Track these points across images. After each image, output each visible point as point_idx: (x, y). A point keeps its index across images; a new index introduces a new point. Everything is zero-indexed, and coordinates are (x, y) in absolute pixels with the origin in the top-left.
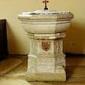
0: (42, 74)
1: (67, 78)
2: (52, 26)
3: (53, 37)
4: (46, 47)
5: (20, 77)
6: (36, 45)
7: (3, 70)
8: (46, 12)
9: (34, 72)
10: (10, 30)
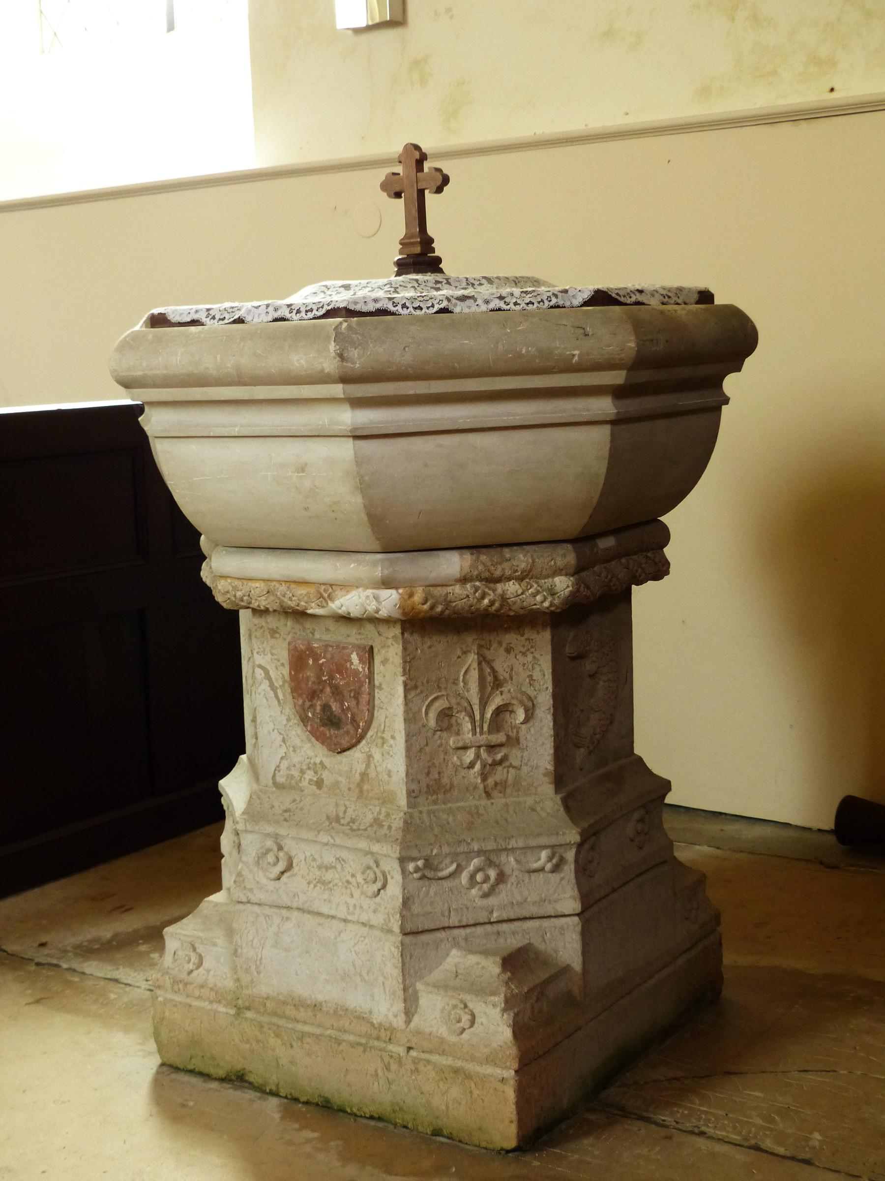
0: (284, 1009)
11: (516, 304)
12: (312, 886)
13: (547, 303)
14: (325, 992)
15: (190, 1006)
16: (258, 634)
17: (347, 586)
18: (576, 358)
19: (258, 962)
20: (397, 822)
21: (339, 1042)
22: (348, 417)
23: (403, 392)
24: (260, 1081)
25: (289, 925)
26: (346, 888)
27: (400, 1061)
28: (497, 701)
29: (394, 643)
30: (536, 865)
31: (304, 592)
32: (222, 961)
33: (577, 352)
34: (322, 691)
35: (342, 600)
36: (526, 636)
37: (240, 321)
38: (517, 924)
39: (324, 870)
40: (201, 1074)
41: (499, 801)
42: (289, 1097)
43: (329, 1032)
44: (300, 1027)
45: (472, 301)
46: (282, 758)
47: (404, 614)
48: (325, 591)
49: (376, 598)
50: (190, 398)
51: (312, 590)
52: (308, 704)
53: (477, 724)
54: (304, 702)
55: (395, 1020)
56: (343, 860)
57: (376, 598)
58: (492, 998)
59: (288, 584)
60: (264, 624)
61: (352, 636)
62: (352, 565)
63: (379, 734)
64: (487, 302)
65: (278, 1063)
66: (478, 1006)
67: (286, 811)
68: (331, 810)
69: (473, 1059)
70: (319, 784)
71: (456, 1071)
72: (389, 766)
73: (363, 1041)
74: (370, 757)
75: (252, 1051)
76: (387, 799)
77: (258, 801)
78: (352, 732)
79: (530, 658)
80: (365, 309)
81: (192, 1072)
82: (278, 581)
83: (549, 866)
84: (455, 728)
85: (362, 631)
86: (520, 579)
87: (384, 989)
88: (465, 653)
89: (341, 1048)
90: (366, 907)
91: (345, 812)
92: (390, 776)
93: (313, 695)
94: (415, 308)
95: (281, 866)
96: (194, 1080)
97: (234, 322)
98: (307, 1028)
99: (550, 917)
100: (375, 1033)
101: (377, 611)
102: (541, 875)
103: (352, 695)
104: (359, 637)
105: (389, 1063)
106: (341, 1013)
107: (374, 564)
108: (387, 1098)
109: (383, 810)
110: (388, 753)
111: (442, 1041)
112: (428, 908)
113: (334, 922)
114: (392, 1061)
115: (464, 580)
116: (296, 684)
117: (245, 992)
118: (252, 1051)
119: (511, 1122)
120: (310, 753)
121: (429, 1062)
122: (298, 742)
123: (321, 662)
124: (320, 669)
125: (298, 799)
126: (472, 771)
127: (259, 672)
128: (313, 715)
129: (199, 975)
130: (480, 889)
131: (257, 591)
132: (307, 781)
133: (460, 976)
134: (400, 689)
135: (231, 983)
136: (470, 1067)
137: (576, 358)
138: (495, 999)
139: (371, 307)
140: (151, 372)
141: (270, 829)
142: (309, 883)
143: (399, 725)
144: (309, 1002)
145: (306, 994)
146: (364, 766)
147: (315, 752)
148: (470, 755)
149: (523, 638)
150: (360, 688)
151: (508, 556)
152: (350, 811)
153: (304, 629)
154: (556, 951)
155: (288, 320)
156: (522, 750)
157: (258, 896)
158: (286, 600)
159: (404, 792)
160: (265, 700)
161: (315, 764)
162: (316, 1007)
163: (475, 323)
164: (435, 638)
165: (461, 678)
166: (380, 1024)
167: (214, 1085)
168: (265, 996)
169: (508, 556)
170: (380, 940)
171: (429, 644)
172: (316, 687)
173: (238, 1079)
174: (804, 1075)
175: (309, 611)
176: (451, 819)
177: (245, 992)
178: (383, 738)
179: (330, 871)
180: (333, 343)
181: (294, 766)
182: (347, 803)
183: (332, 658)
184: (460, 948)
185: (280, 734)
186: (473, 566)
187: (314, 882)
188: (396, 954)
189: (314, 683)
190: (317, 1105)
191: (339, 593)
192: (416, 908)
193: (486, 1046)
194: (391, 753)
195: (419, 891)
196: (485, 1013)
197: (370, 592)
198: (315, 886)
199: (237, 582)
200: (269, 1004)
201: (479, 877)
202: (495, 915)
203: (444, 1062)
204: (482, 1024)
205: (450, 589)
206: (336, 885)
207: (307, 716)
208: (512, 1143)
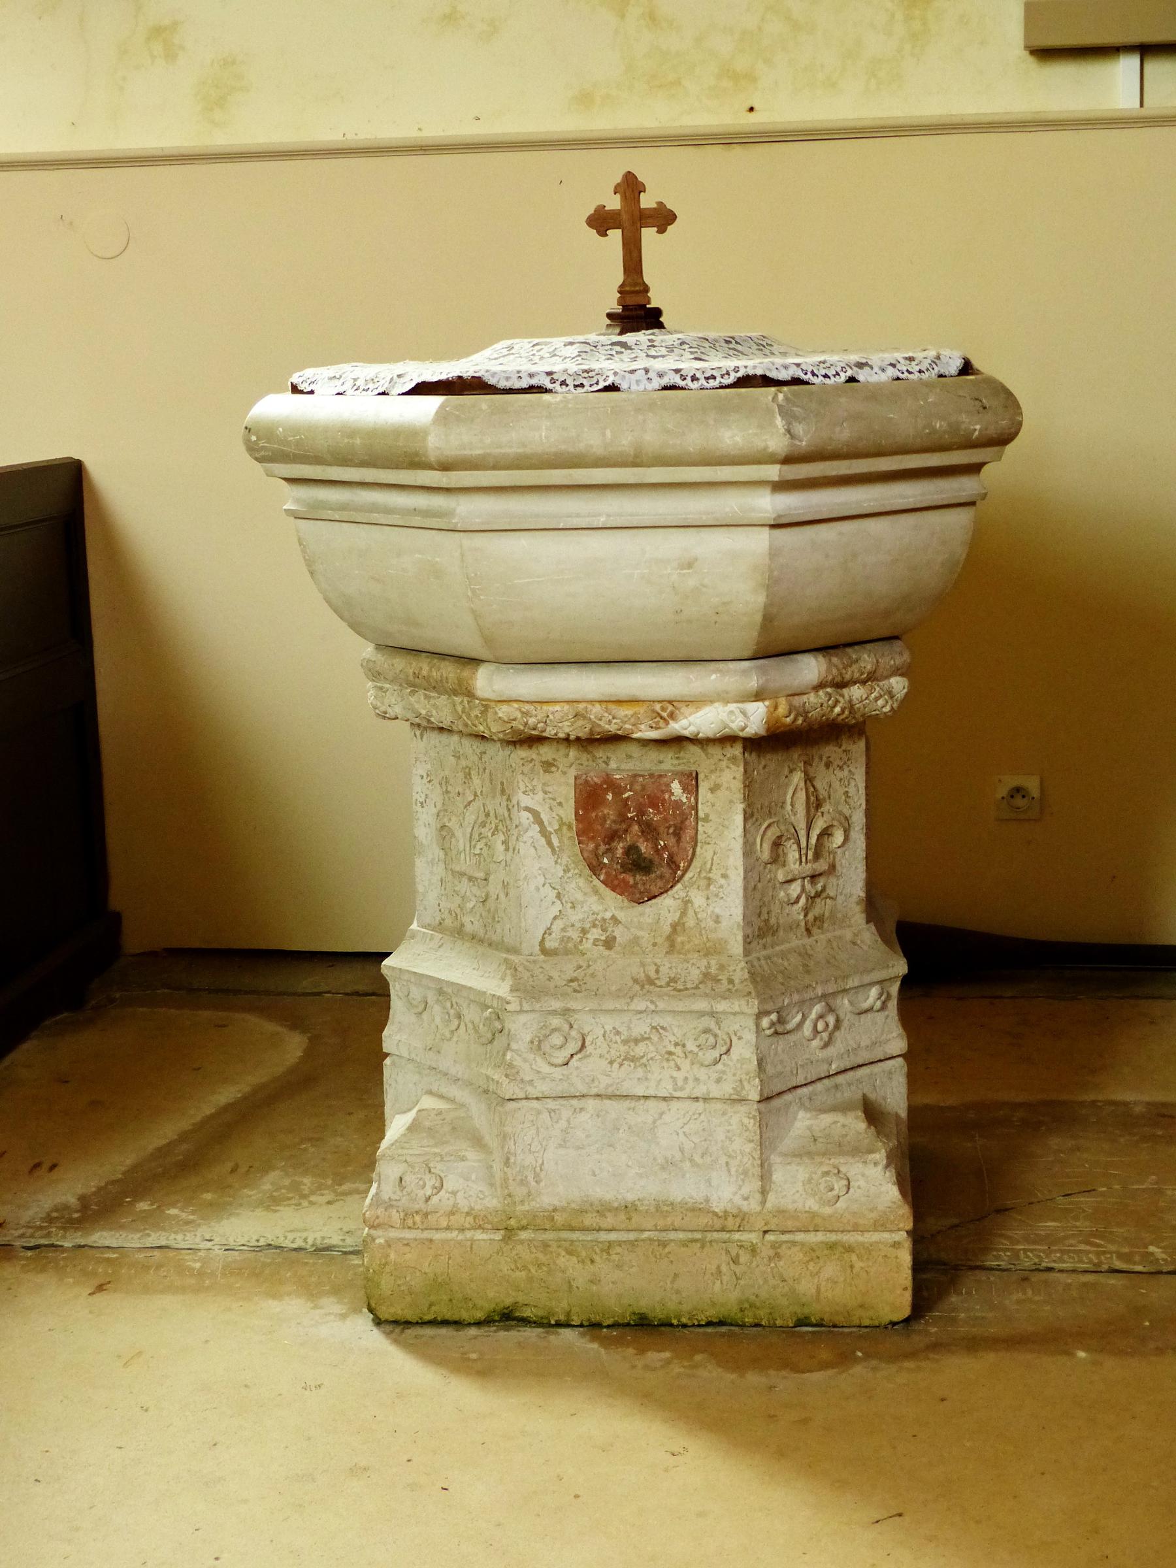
0: (573, 1224)
1: (940, 1265)
2: (722, 554)
3: (725, 704)
4: (633, 844)
5: (273, 1268)
6: (502, 824)
7: (41, 1167)
8: (643, 360)
9: (465, 1185)
10: (93, 491)
12: (616, 1065)
13: (842, 374)
14: (639, 1186)
15: (431, 1240)
16: (526, 769)
18: (977, 433)
19: (538, 1169)
20: (739, 972)
21: (664, 1244)
22: (768, 504)
23: (873, 469)
24: (541, 1313)
25: (584, 1117)
26: (668, 1060)
27: (753, 1250)
28: (819, 825)
30: (866, 1005)
31: (630, 712)
32: (473, 1177)
33: (978, 427)
34: (626, 831)
35: (691, 718)
36: (843, 748)
37: (612, 388)
38: (851, 1074)
39: (632, 1044)
40: (445, 1323)
41: (821, 937)
42: (585, 1323)
43: (646, 1235)
44: (604, 1236)
46: (555, 918)
47: (768, 730)
48: (663, 709)
49: (744, 713)
51: (641, 710)
52: (603, 848)
53: (803, 852)
54: (597, 847)
55: (745, 1203)
56: (662, 1028)
57: (744, 713)
58: (873, 1156)
59: (604, 705)
60: (534, 756)
61: (668, 761)
62: (714, 677)
63: (703, 874)
64: (661, 375)
65: (570, 1286)
66: (853, 1168)
67: (571, 981)
68: (636, 971)
69: (856, 1228)
70: (609, 943)
71: (832, 1246)
72: (717, 910)
73: (698, 1236)
74: (687, 902)
75: (530, 1279)
76: (712, 949)
77: (528, 974)
78: (667, 875)
79: (846, 772)
80: (518, 385)
81: (433, 1323)
82: (592, 702)
83: (878, 1004)
84: (782, 859)
85: (682, 754)
86: (864, 682)
87: (729, 1171)
88: (791, 771)
89: (667, 1250)
91: (657, 971)
93: (612, 837)
94: (707, 379)
95: (573, 1046)
96: (443, 1331)
97: (665, 388)
98: (613, 1236)
99: (880, 1061)
101: (743, 729)
102: (869, 1015)
103: (671, 831)
104: (676, 762)
105: (738, 1255)
106: (666, 1208)
107: (745, 672)
108: (733, 1296)
109: (713, 962)
110: (717, 895)
111: (813, 1215)
112: (779, 1068)
113: (651, 1103)
114: (741, 1252)
115: (818, 687)
116: (586, 827)
117: (519, 1208)
118: (530, 1279)
119: (905, 1289)
120: (596, 907)
121: (794, 1243)
122: (579, 896)
125: (585, 965)
126: (796, 907)
127: (525, 818)
128: (611, 860)
129: (442, 1200)
130: (821, 1039)
131: (558, 716)
133: (820, 1140)
134: (739, 819)
135: (495, 1201)
137: (977, 433)
138: (877, 1156)
139: (524, 384)
140: (498, 451)
141: (556, 1005)
142: (611, 1063)
143: (735, 864)
144: (616, 1205)
145: (609, 1196)
146: (678, 914)
147: (611, 904)
148: (795, 889)
149: (840, 750)
150: (682, 822)
151: (854, 657)
153: (594, 759)
154: (885, 1099)
156: (838, 877)
157: (542, 1088)
158: (601, 723)
159: (740, 938)
160: (533, 850)
161: (604, 920)
162: (629, 1209)
163: (875, 394)
164: (769, 756)
165: (789, 800)
166: (726, 1212)
167: (473, 1331)
168: (551, 1208)
169: (854, 657)
171: (763, 763)
172: (615, 827)
173: (507, 1318)
174: (1068, 1199)
175: (634, 736)
176: (786, 964)
177: (519, 1208)
179: (641, 1044)
180: (779, 418)
181: (573, 925)
182: (658, 961)
183: (644, 788)
184: (807, 1110)
186: (828, 670)
187: (619, 1060)
188: (750, 1126)
189: (614, 822)
190: (628, 1325)
191: (684, 709)
192: (770, 1070)
193: (871, 1210)
194: (721, 895)
195: (769, 1048)
196: (863, 1175)
197: (732, 706)
198: (621, 1065)
199: (527, 707)
201: (820, 1026)
202: (834, 1066)
204: (859, 1187)
205: (805, 698)
207: (601, 864)
208: (906, 1312)
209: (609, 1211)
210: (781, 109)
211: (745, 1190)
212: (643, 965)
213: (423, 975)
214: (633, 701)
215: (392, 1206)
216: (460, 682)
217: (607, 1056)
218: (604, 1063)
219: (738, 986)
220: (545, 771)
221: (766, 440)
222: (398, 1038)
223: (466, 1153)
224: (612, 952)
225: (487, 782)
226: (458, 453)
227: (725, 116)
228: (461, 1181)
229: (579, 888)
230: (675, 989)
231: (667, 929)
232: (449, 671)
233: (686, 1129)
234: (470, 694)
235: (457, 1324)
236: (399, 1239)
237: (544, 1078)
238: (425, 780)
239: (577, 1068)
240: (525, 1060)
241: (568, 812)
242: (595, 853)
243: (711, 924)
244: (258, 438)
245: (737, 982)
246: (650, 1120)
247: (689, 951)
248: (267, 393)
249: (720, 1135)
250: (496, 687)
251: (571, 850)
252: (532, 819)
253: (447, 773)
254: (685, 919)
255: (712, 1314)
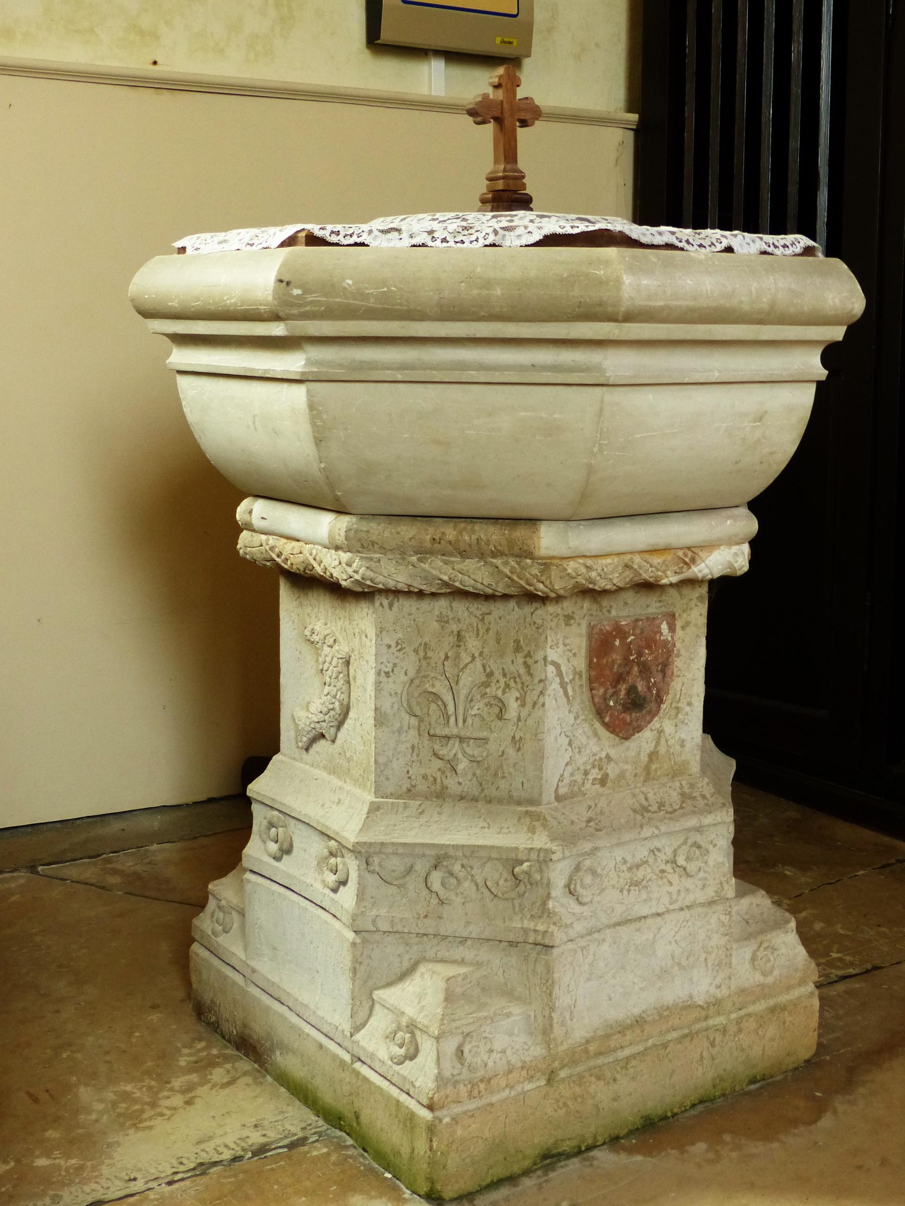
11: (444, 240)
12: (625, 892)
14: (641, 1000)
15: (492, 1105)
17: (710, 546)
21: (665, 1046)
24: (574, 1143)
25: (605, 947)
26: (661, 878)
29: (699, 604)
32: (516, 1031)
34: (628, 673)
39: (634, 870)
45: (396, 233)
46: (567, 764)
48: (686, 555)
50: (689, 337)
51: (669, 557)
54: (605, 692)
60: (559, 611)
62: (729, 522)
72: (683, 736)
73: (686, 1031)
74: (661, 732)
76: (678, 772)
85: (664, 597)
87: (706, 966)
89: (667, 1051)
90: (692, 887)
91: (646, 799)
92: (682, 746)
93: (619, 678)
98: (627, 1052)
100: (703, 1013)
104: (659, 605)
106: (665, 1014)
109: (684, 783)
111: (763, 986)
113: (650, 921)
120: (595, 749)
121: (750, 1015)
123: (629, 640)
124: (628, 648)
125: (593, 805)
131: (610, 568)
132: (590, 782)
133: (750, 921)
135: (538, 1049)
136: (783, 999)
140: (675, 303)
142: (621, 891)
144: (629, 1022)
146: (654, 744)
150: (668, 659)
152: (650, 796)
155: (499, 246)
158: (641, 572)
161: (601, 759)
162: (639, 1022)
166: (707, 1003)
168: (583, 1041)
170: (706, 915)
172: (621, 671)
178: (677, 708)
179: (641, 868)
181: (579, 769)
183: (642, 632)
185: (567, 736)
187: (627, 887)
189: (620, 665)
194: (686, 721)
196: (784, 943)
198: (629, 891)
199: (589, 562)
200: (592, 1048)
203: (761, 1008)
206: (650, 879)
209: (627, 1029)
210: (179, 63)
211: (718, 980)
212: (634, 795)
213: (415, 844)
214: (666, 549)
215: (457, 1082)
216: (511, 543)
217: (617, 885)
218: (616, 893)
219: (712, 800)
220: (566, 625)
221: (853, 303)
222: (374, 912)
223: (511, 1009)
224: (605, 789)
225: (492, 642)
226: (647, 303)
227: (134, 62)
228: (507, 1037)
229: (584, 732)
230: (667, 812)
231: (644, 758)
232: (493, 535)
233: (677, 937)
234: (530, 555)
235: (511, 1179)
236: (465, 1113)
237: (578, 919)
238: (393, 649)
239: (599, 902)
240: (562, 906)
241: (581, 663)
242: (605, 699)
243: (678, 747)
244: (306, 291)
245: (708, 796)
246: (651, 936)
247: (660, 777)
248: (147, 258)
249: (702, 935)
250: (571, 544)
251: (581, 698)
252: (555, 672)
253: (426, 639)
254: (659, 748)
255: (694, 1098)
